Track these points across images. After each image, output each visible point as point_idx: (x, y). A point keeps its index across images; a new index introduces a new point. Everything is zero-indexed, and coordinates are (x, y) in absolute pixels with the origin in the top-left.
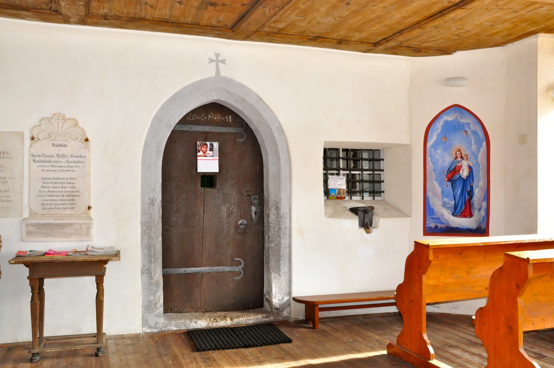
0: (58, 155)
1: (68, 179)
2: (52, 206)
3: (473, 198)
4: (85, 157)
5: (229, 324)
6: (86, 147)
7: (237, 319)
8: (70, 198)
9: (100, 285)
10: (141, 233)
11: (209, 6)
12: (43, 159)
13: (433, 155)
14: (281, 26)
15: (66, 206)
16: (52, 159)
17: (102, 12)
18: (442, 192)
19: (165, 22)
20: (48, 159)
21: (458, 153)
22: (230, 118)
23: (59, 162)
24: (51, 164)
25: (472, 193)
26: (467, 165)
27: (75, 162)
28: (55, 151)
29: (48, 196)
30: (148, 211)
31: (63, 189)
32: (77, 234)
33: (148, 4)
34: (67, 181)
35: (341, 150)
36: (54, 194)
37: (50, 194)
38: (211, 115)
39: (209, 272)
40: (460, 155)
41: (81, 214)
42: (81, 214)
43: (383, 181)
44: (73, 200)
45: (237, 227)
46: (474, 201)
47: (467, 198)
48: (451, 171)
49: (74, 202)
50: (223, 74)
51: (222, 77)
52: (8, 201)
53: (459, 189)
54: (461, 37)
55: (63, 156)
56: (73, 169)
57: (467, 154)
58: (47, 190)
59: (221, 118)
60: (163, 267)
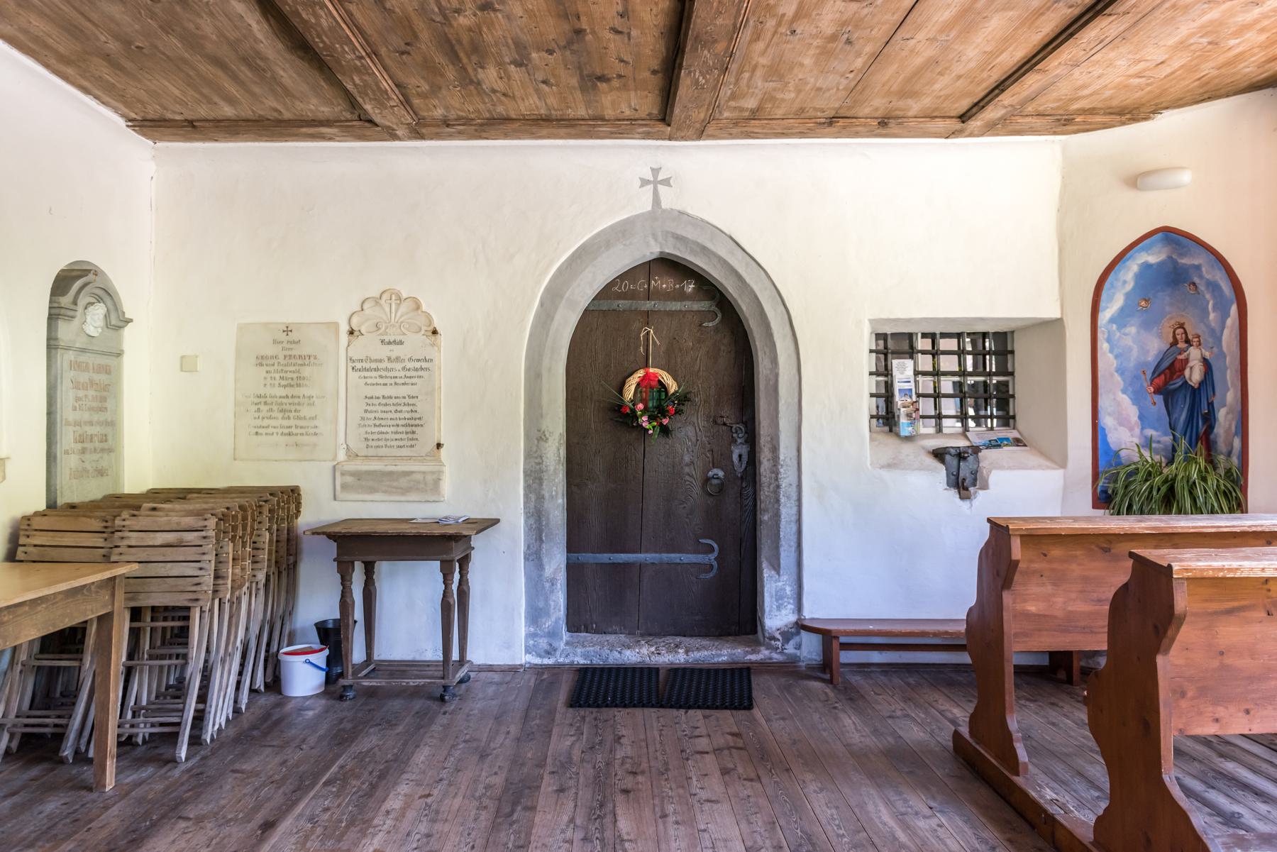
0: (389, 359)
1: (404, 398)
2: (380, 443)
3: (1215, 430)
4: (431, 360)
5: (682, 661)
6: (433, 345)
7: (695, 653)
8: (409, 429)
9: (449, 578)
10: (525, 490)
11: (599, 84)
12: (367, 365)
13: (1116, 337)
14: (751, 103)
15: (401, 443)
16: (381, 366)
17: (439, 113)
18: (1141, 417)
19: (543, 120)
20: (374, 365)
21: (1180, 331)
22: (690, 287)
23: (392, 370)
24: (379, 373)
25: (1213, 419)
26: (1199, 356)
27: (416, 370)
28: (385, 351)
29: (375, 425)
30: (536, 451)
31: (398, 415)
32: (418, 489)
33: (497, 91)
34: (404, 401)
35: (920, 335)
36: (383, 422)
37: (378, 422)
38: (656, 281)
39: (653, 563)
40: (1184, 335)
41: (427, 456)
42: (427, 456)
43: (872, 395)
44: (414, 432)
45: (707, 480)
46: (1216, 436)
47: (1202, 429)
48: (1163, 372)
49: (415, 436)
50: (665, 205)
51: (664, 211)
52: (316, 434)
53: (1183, 409)
54: (1152, 80)
55: (398, 359)
56: (413, 381)
57: (1199, 332)
58: (372, 416)
59: (675, 285)
60: (570, 549)
